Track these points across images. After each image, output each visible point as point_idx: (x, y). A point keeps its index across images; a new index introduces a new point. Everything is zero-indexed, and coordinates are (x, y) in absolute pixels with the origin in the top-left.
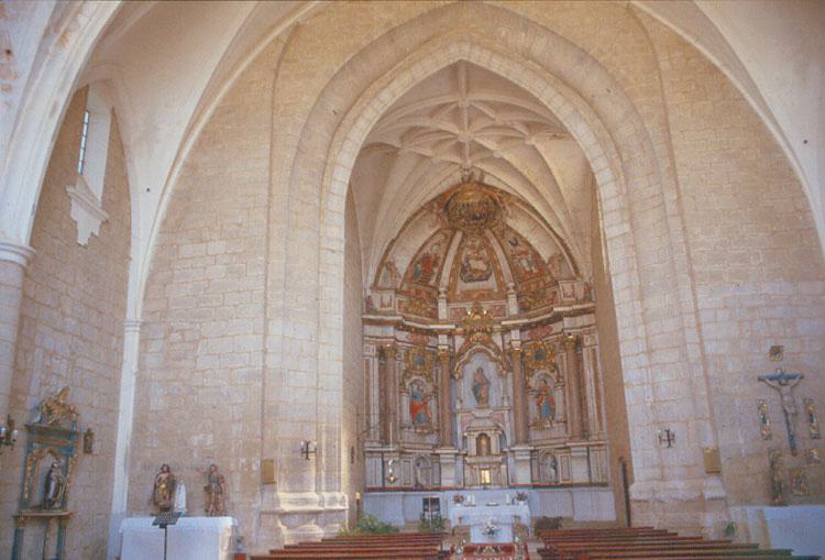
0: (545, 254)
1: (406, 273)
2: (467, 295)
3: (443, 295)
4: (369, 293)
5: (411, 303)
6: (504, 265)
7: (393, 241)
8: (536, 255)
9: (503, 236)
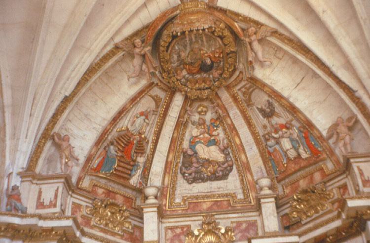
0: (322, 121)
1: (89, 159)
2: (192, 206)
3: (152, 201)
4: (16, 181)
5: (95, 211)
6: (252, 154)
7: (67, 100)
8: (308, 126)
9: (249, 103)
